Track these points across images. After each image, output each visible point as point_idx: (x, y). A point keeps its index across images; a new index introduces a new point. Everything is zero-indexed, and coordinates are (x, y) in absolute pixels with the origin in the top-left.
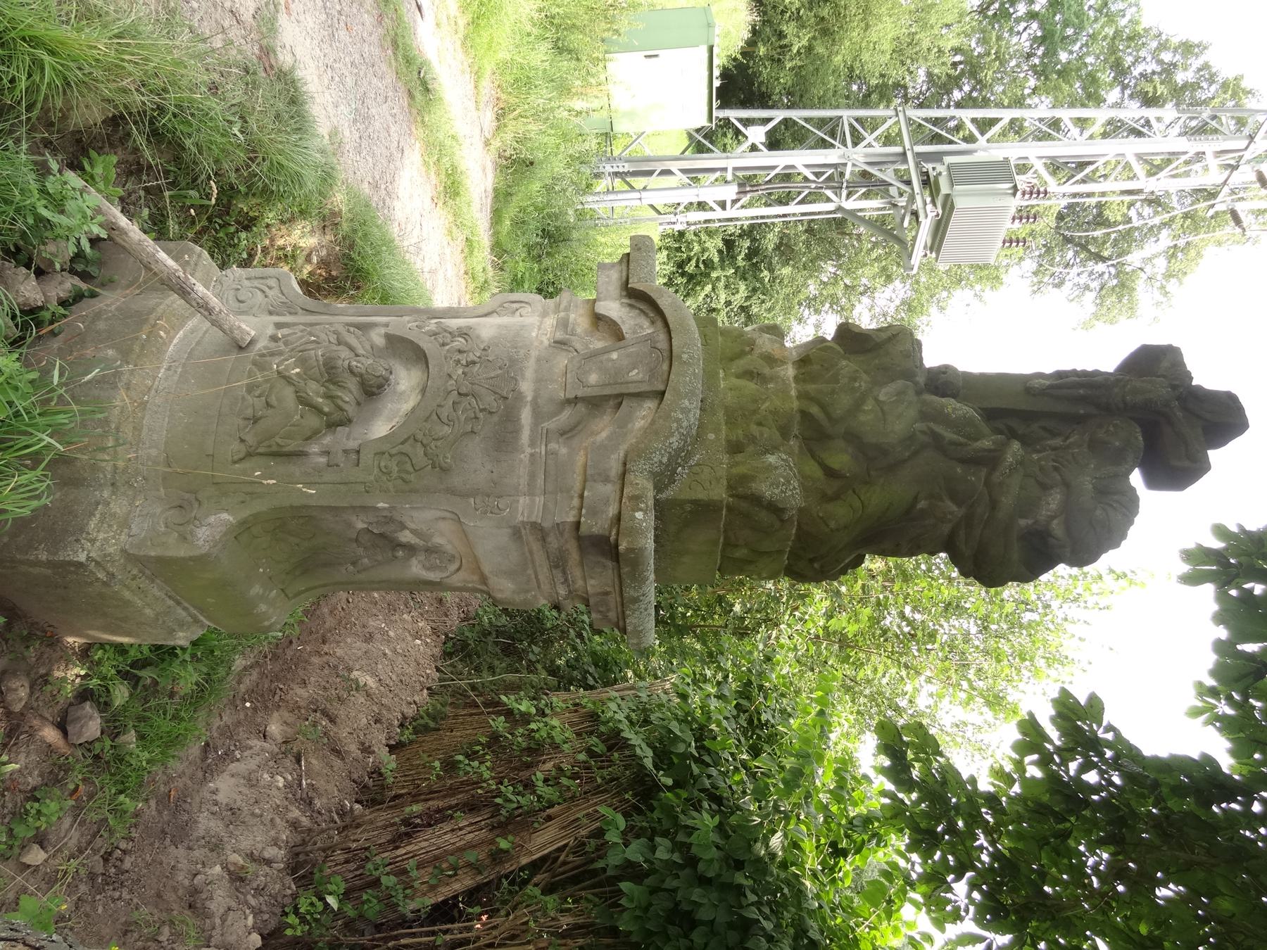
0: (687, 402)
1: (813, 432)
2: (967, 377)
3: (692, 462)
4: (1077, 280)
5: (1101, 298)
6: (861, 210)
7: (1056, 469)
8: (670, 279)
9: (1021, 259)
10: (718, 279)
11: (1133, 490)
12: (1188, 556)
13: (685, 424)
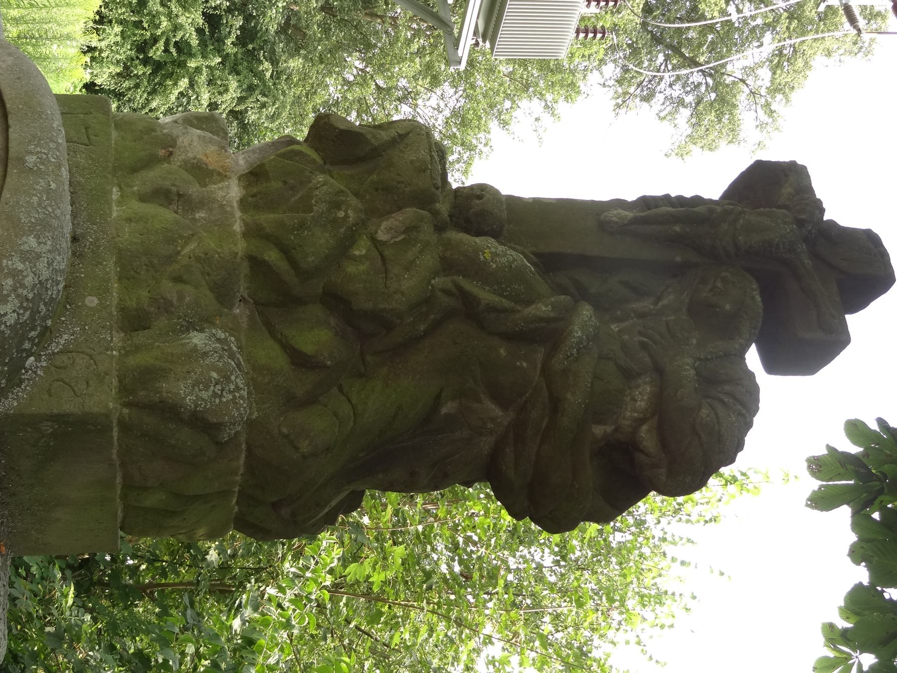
0: (32, 241)
1: (275, 287)
2: (513, 202)
3: (54, 348)
4: (669, 91)
5: (697, 114)
8: (126, 68)
9: (602, 62)
10: (198, 70)
11: (751, 376)
12: (817, 466)
13: (29, 280)
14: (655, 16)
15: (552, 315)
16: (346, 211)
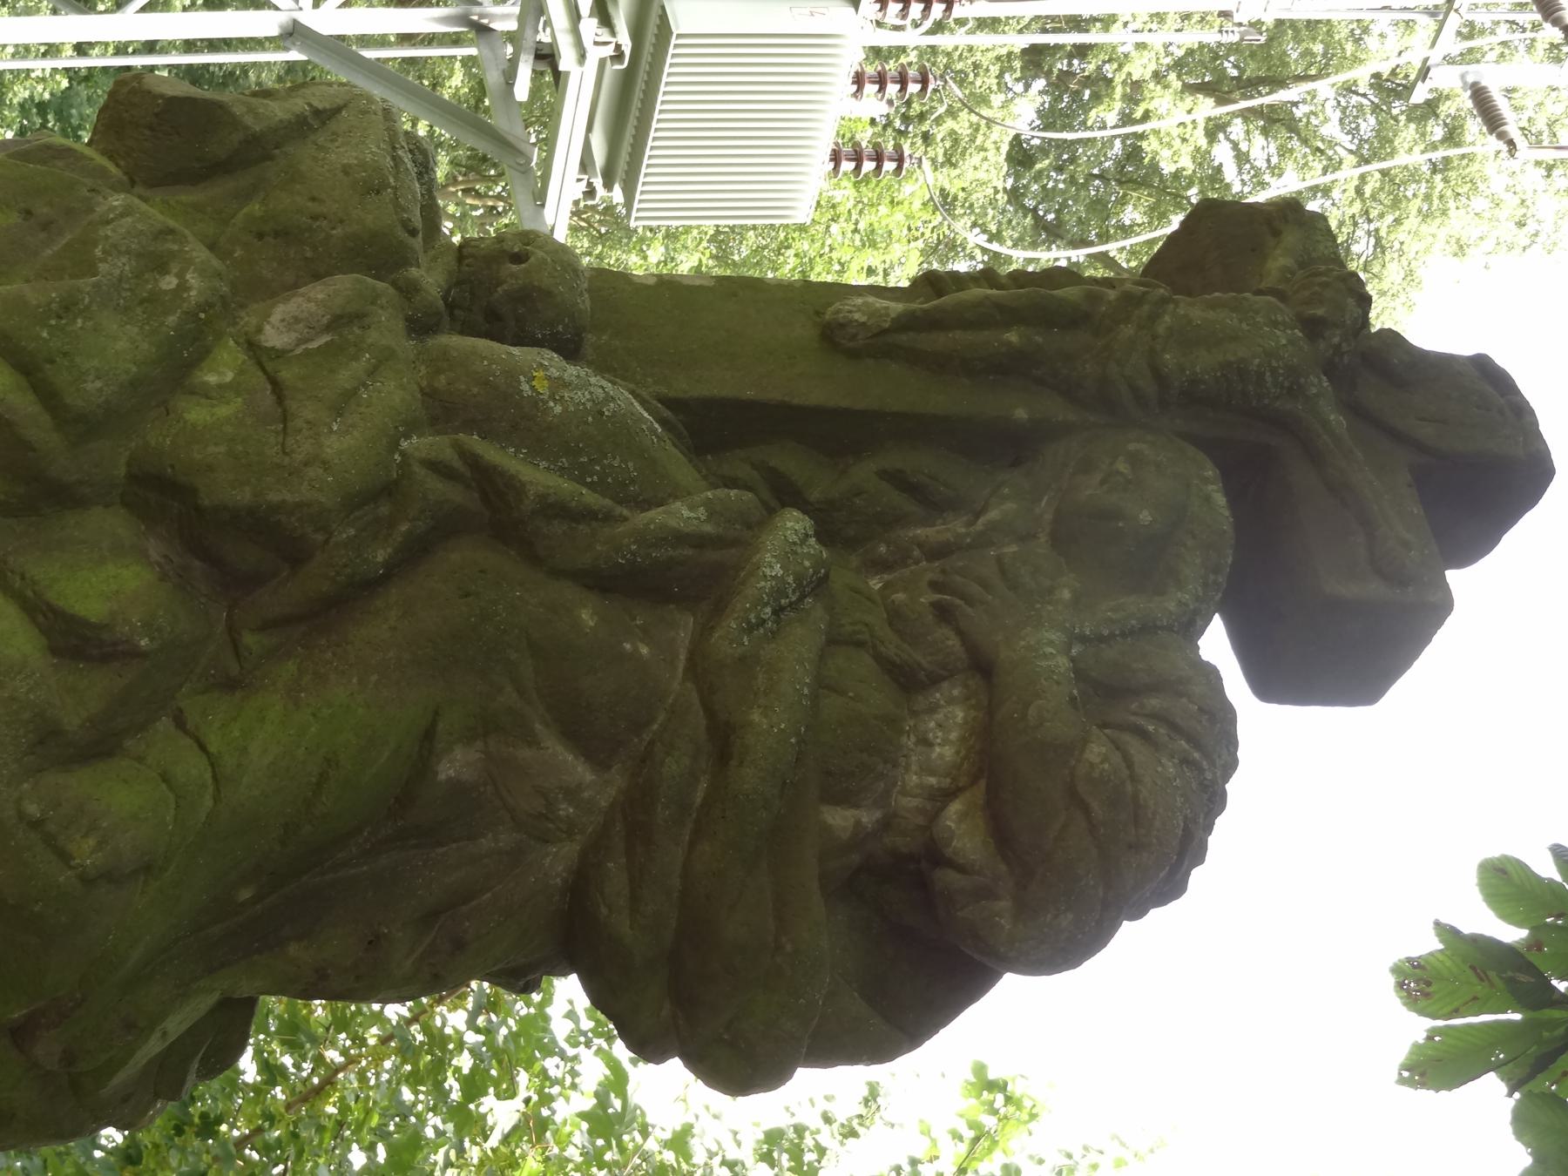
6: (366, 41)
7: (943, 613)
12: (1419, 983)
14: (1040, 172)
15: (708, 528)
16: (181, 276)
